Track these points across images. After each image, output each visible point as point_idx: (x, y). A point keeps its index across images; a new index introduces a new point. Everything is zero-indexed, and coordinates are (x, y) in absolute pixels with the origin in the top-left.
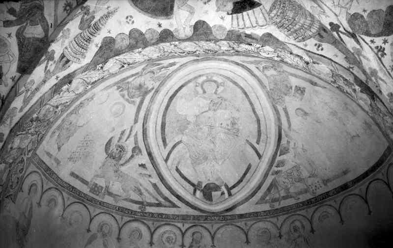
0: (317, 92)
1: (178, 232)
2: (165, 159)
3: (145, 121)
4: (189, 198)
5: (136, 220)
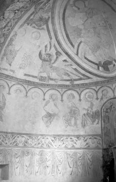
2: (76, 54)
3: (56, 36)
4: (96, 72)
5: (70, 89)
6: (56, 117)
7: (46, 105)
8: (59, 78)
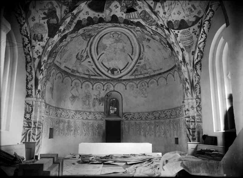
0: (154, 41)
1: (102, 85)
4: (106, 73)
6: (77, 99)
7: (72, 89)
8: (83, 73)
